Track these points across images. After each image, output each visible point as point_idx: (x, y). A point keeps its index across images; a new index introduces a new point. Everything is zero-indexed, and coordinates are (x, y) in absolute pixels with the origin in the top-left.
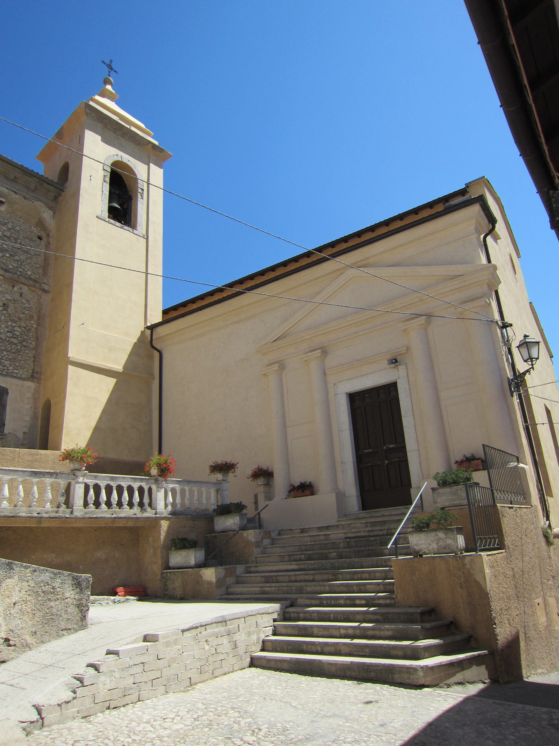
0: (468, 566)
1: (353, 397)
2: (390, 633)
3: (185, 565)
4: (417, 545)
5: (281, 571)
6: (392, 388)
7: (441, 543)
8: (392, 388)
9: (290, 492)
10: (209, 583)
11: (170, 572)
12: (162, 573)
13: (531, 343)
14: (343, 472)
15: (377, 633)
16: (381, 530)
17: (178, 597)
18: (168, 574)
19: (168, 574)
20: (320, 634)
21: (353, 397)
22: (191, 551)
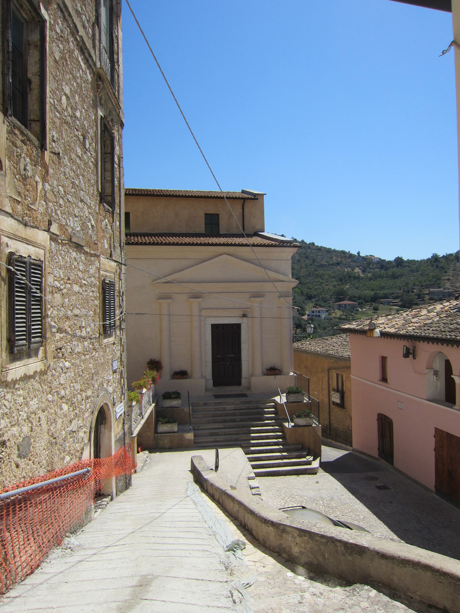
0: (316, 430)
1: (214, 327)
2: (295, 456)
3: (170, 431)
4: (298, 422)
5: (214, 429)
6: (238, 326)
7: (308, 422)
8: (238, 326)
9: (173, 375)
10: (190, 440)
11: (160, 436)
12: (154, 436)
13: (184, 231)
14: (206, 367)
15: (290, 457)
16: (253, 407)
17: (167, 448)
18: (159, 437)
19: (159, 437)
20: (265, 459)
21: (214, 327)
22: (175, 425)
